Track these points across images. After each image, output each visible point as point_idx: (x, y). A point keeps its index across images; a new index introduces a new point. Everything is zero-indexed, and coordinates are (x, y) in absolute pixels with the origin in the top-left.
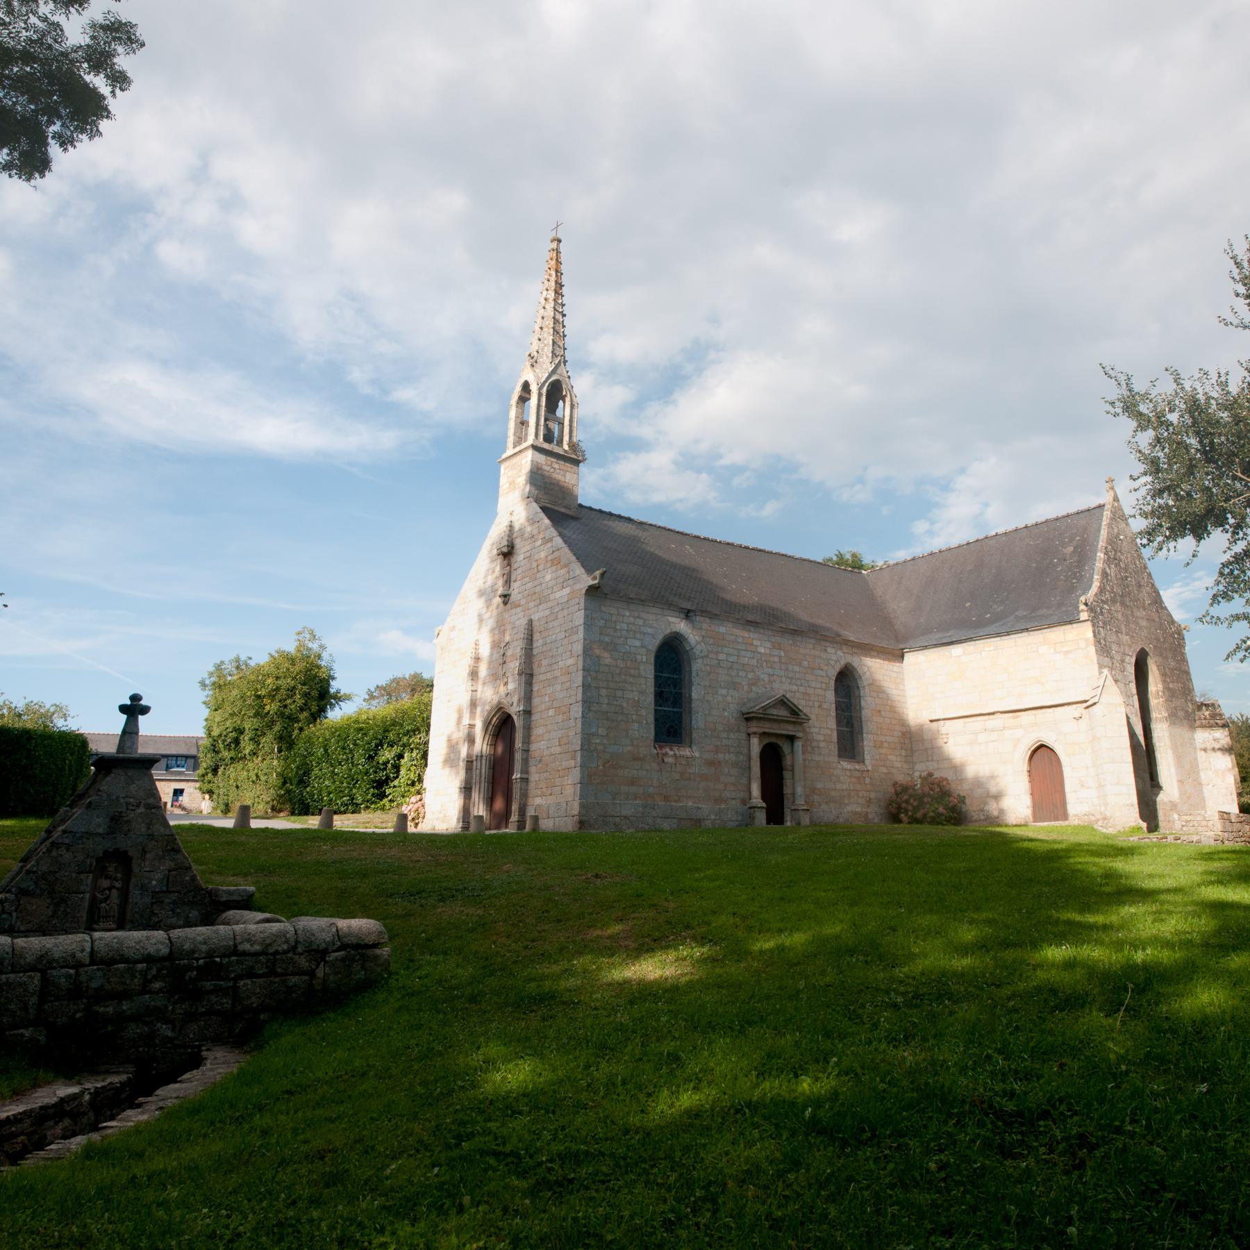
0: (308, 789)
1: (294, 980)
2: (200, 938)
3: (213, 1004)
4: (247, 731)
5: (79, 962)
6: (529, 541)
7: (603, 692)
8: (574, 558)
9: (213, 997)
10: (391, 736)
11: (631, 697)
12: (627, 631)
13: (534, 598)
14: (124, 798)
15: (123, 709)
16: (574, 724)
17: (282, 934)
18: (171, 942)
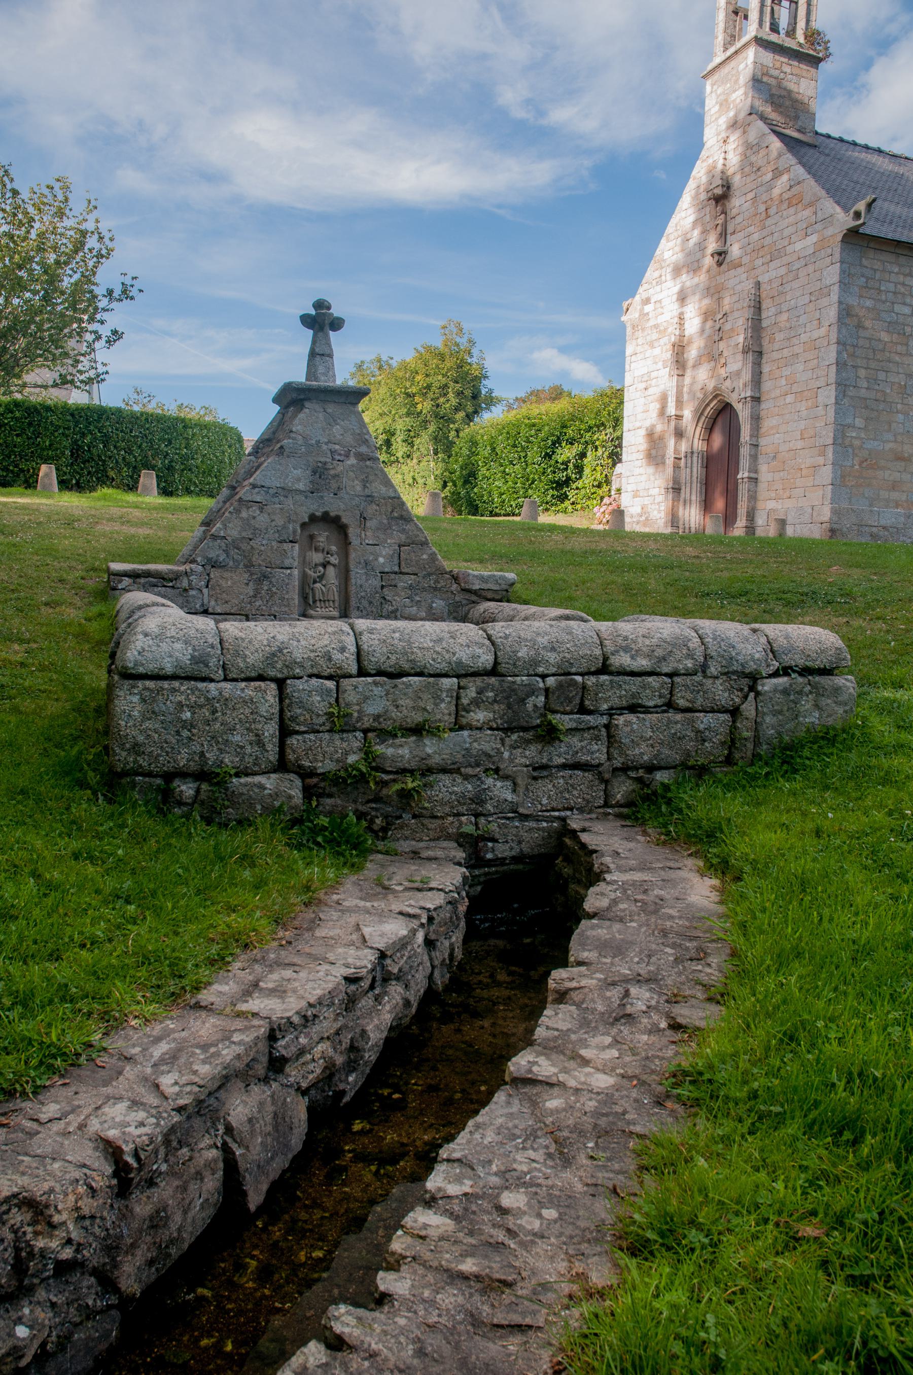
0: (476, 490)
1: (705, 720)
2: (543, 641)
3: (577, 753)
4: (398, 432)
5: (340, 668)
6: (753, 177)
7: (862, 373)
8: (823, 193)
9: (575, 739)
10: (570, 432)
11: (897, 380)
12: (895, 293)
13: (761, 254)
14: (326, 444)
15: (307, 321)
16: (823, 413)
17: (681, 643)
18: (493, 643)
